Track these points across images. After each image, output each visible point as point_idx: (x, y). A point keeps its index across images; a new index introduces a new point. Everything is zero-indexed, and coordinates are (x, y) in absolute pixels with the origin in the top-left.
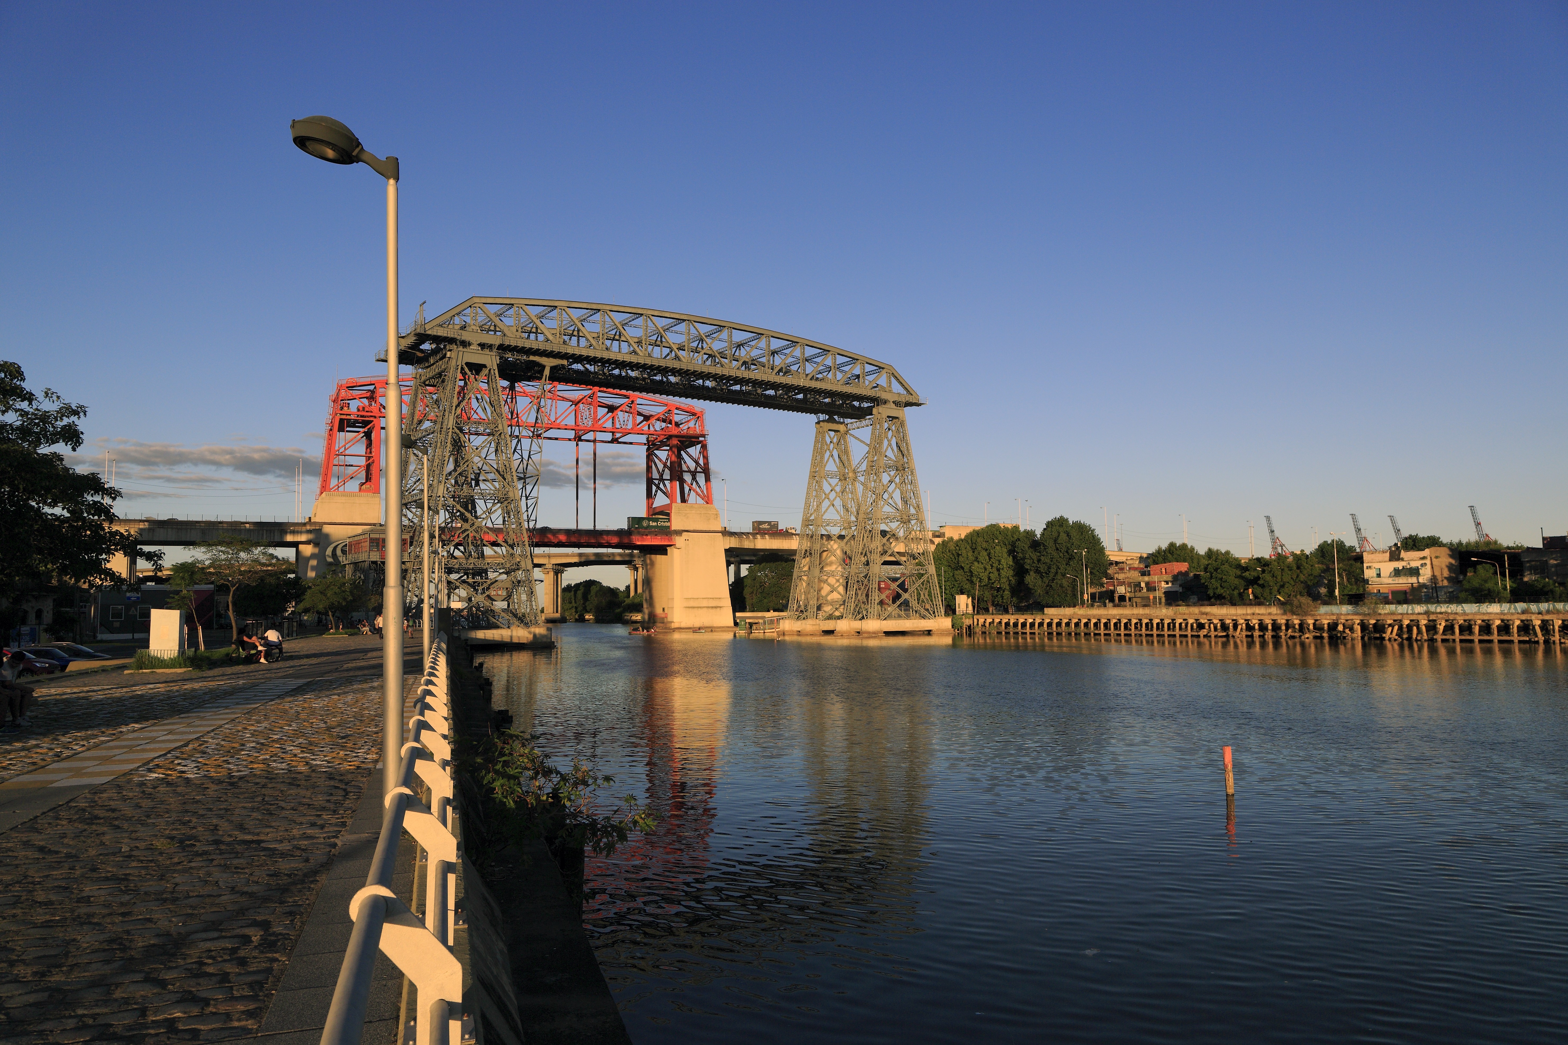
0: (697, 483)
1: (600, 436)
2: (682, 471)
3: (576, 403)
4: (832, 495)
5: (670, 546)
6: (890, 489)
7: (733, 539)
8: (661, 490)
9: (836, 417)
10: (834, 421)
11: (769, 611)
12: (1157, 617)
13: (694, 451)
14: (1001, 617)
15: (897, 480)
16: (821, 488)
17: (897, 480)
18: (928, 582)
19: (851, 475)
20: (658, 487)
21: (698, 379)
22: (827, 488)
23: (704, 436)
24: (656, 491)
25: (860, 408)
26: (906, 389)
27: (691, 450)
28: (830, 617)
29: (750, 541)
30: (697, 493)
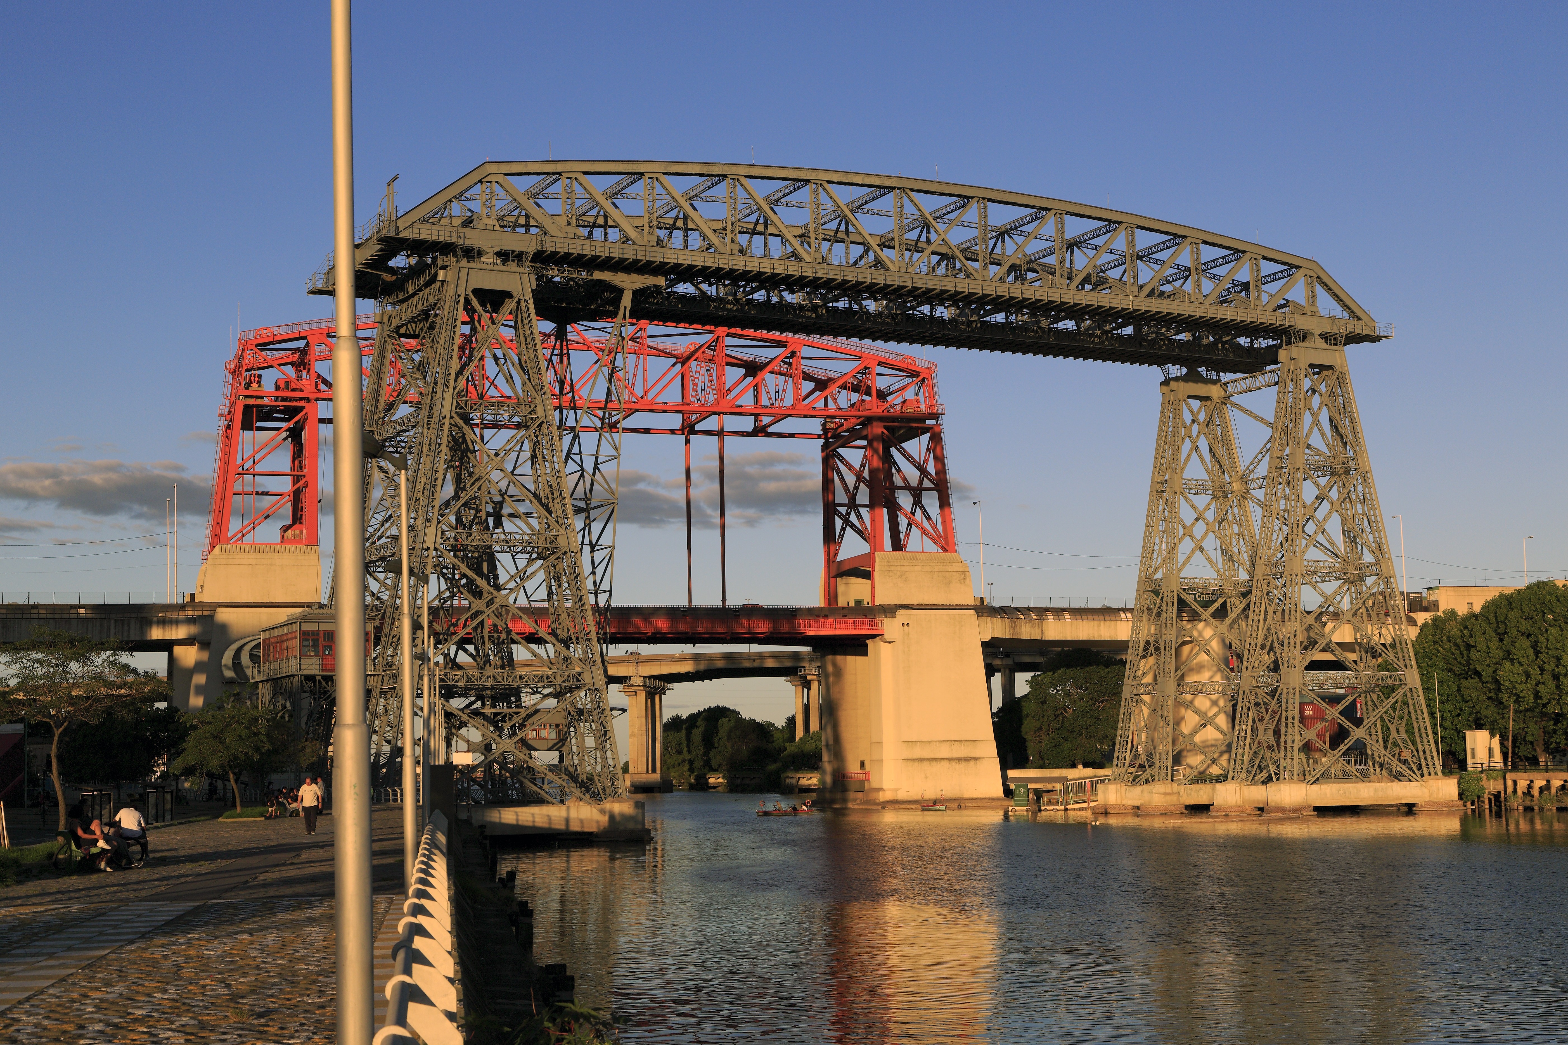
1: (732, 423)
2: (893, 488)
3: (683, 360)
4: (1199, 529)
6: (1320, 514)
7: (997, 621)
8: (853, 527)
9: (1202, 370)
10: (1200, 379)
11: (1073, 766)
13: (917, 447)
15: (1334, 494)
16: (1175, 513)
17: (1334, 494)
19: (1236, 486)
20: (846, 521)
21: (921, 304)
22: (1187, 514)
23: (935, 416)
24: (843, 529)
25: (1251, 350)
26: (1347, 307)
27: (911, 446)
29: (1033, 626)
30: (924, 531)
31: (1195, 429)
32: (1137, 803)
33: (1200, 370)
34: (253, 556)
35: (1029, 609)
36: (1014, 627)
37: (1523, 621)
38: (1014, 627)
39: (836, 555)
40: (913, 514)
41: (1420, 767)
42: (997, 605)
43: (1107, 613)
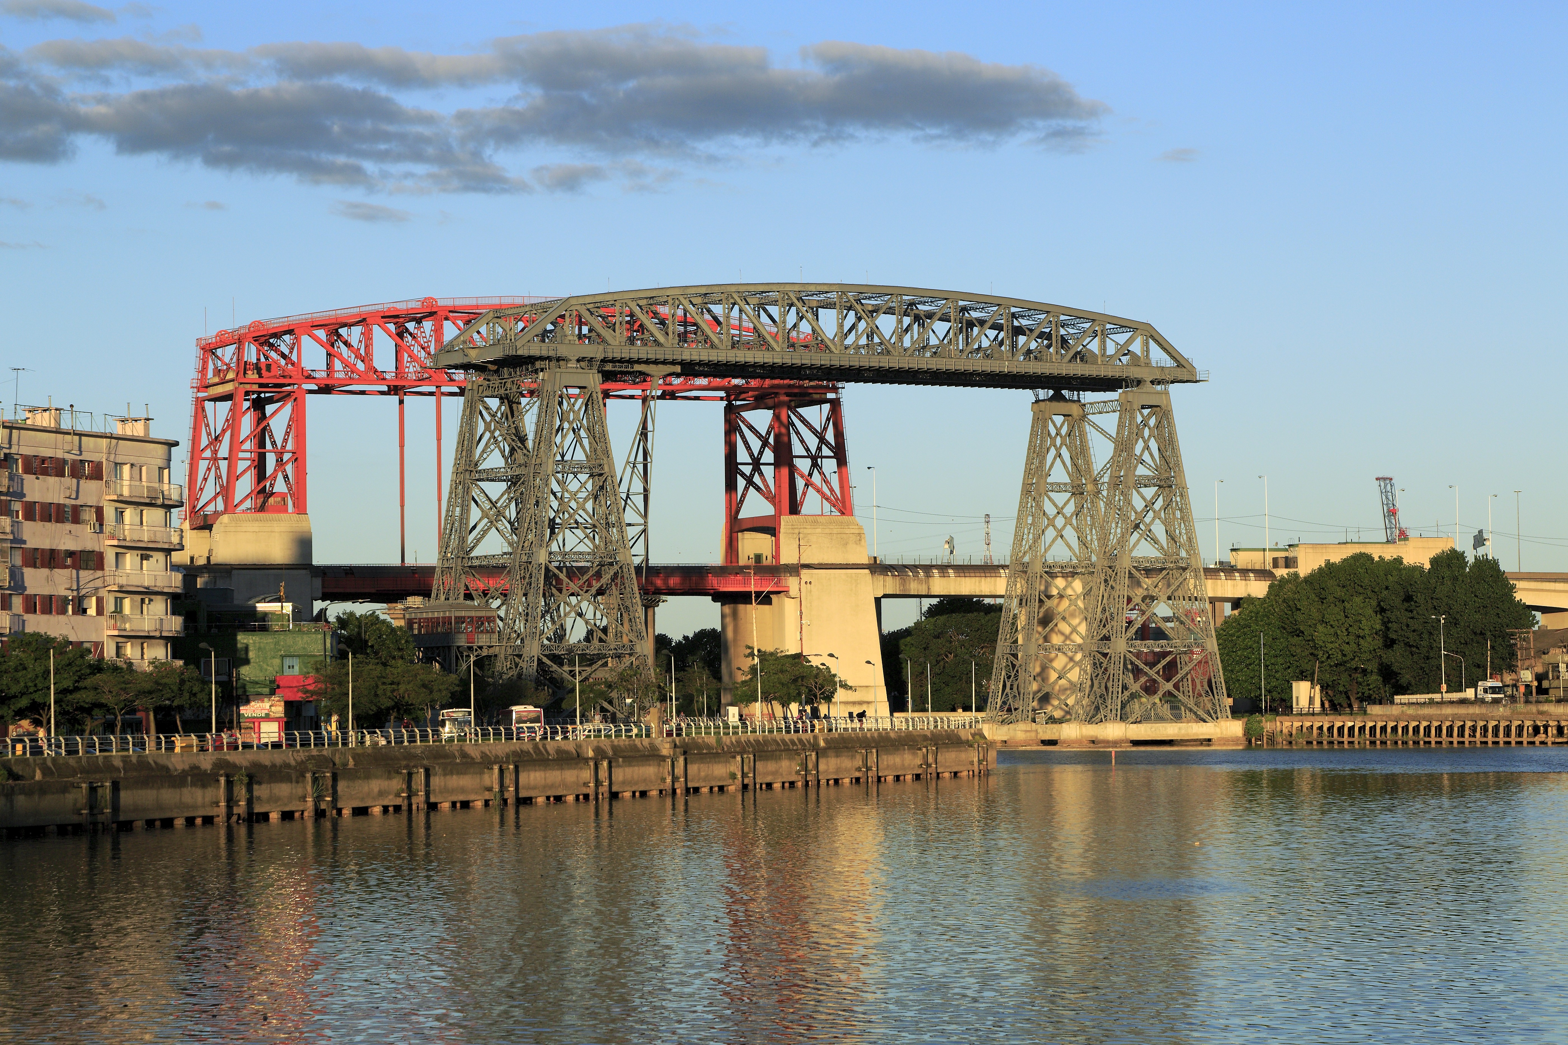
0: (822, 473)
5: (778, 593)
6: (1147, 520)
7: (889, 579)
8: (758, 489)
9: (1065, 392)
10: (1063, 399)
11: (954, 710)
12: (1493, 718)
14: (1331, 718)
16: (1039, 507)
18: (1206, 662)
19: (1090, 487)
20: (750, 482)
24: (746, 489)
26: (1172, 357)
28: (1052, 720)
29: (920, 581)
30: (819, 491)
31: (1058, 441)
32: (1005, 738)
33: (1063, 392)
34: (257, 524)
35: (916, 566)
36: (904, 583)
37: (1338, 589)
38: (904, 583)
39: (738, 512)
40: (810, 475)
41: (1216, 713)
42: (888, 562)
43: (988, 569)
